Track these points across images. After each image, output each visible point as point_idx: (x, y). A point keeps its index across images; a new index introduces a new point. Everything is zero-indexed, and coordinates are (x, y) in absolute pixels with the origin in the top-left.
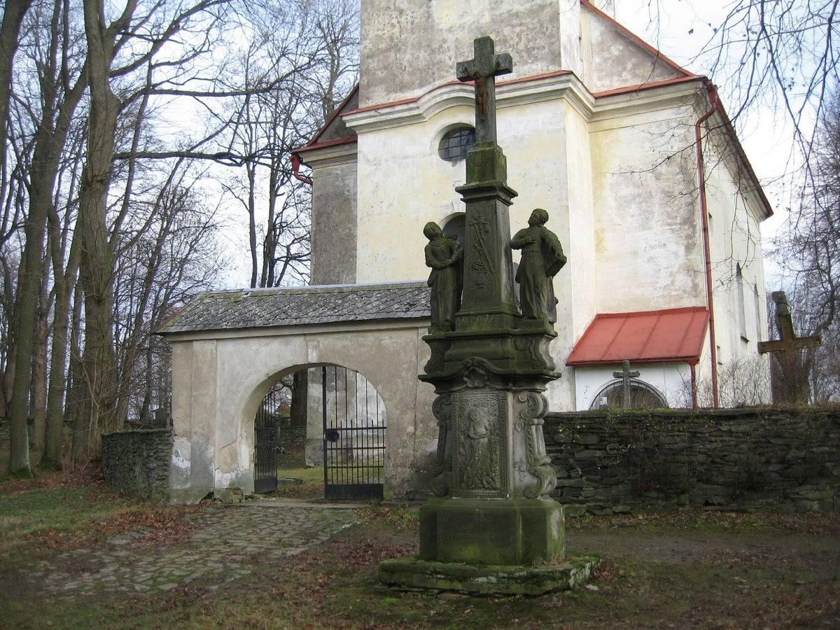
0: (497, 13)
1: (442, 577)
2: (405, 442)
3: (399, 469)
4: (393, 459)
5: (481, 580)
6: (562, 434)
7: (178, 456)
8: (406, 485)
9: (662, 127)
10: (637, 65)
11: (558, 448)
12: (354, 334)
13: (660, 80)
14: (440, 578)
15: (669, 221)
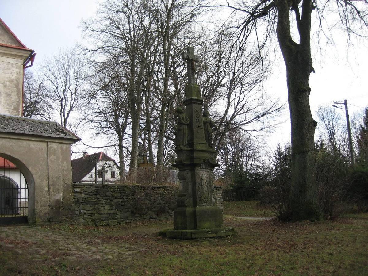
1: (210, 233)
2: (44, 195)
3: (43, 208)
4: (39, 203)
5: (222, 232)
8: (47, 215)
9: (9, 65)
11: (107, 198)
12: (17, 140)
13: (10, 44)
14: (210, 233)
15: (8, 107)
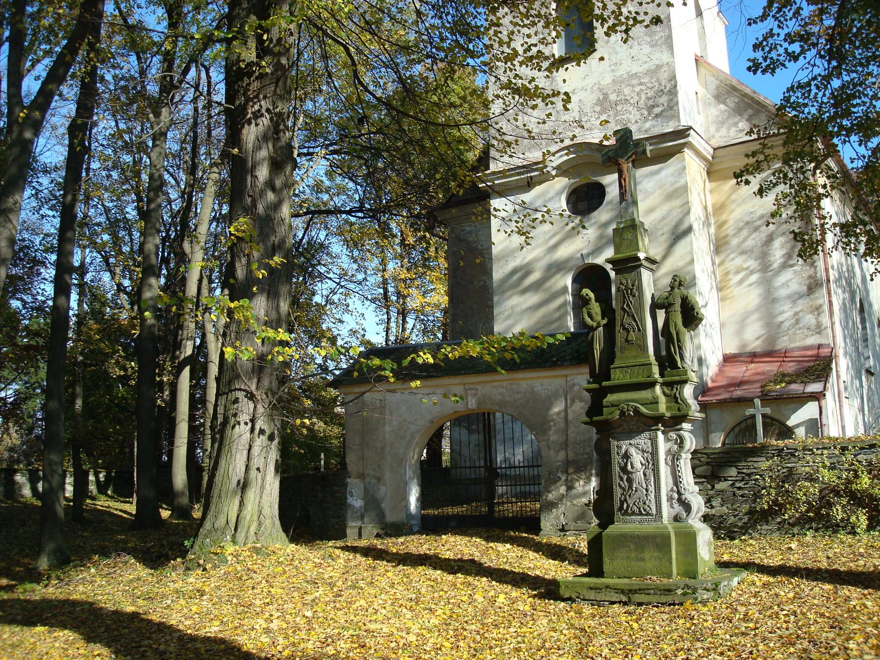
0: (618, 74)
6: (749, 421)
7: (352, 496)
10: (753, 115)
